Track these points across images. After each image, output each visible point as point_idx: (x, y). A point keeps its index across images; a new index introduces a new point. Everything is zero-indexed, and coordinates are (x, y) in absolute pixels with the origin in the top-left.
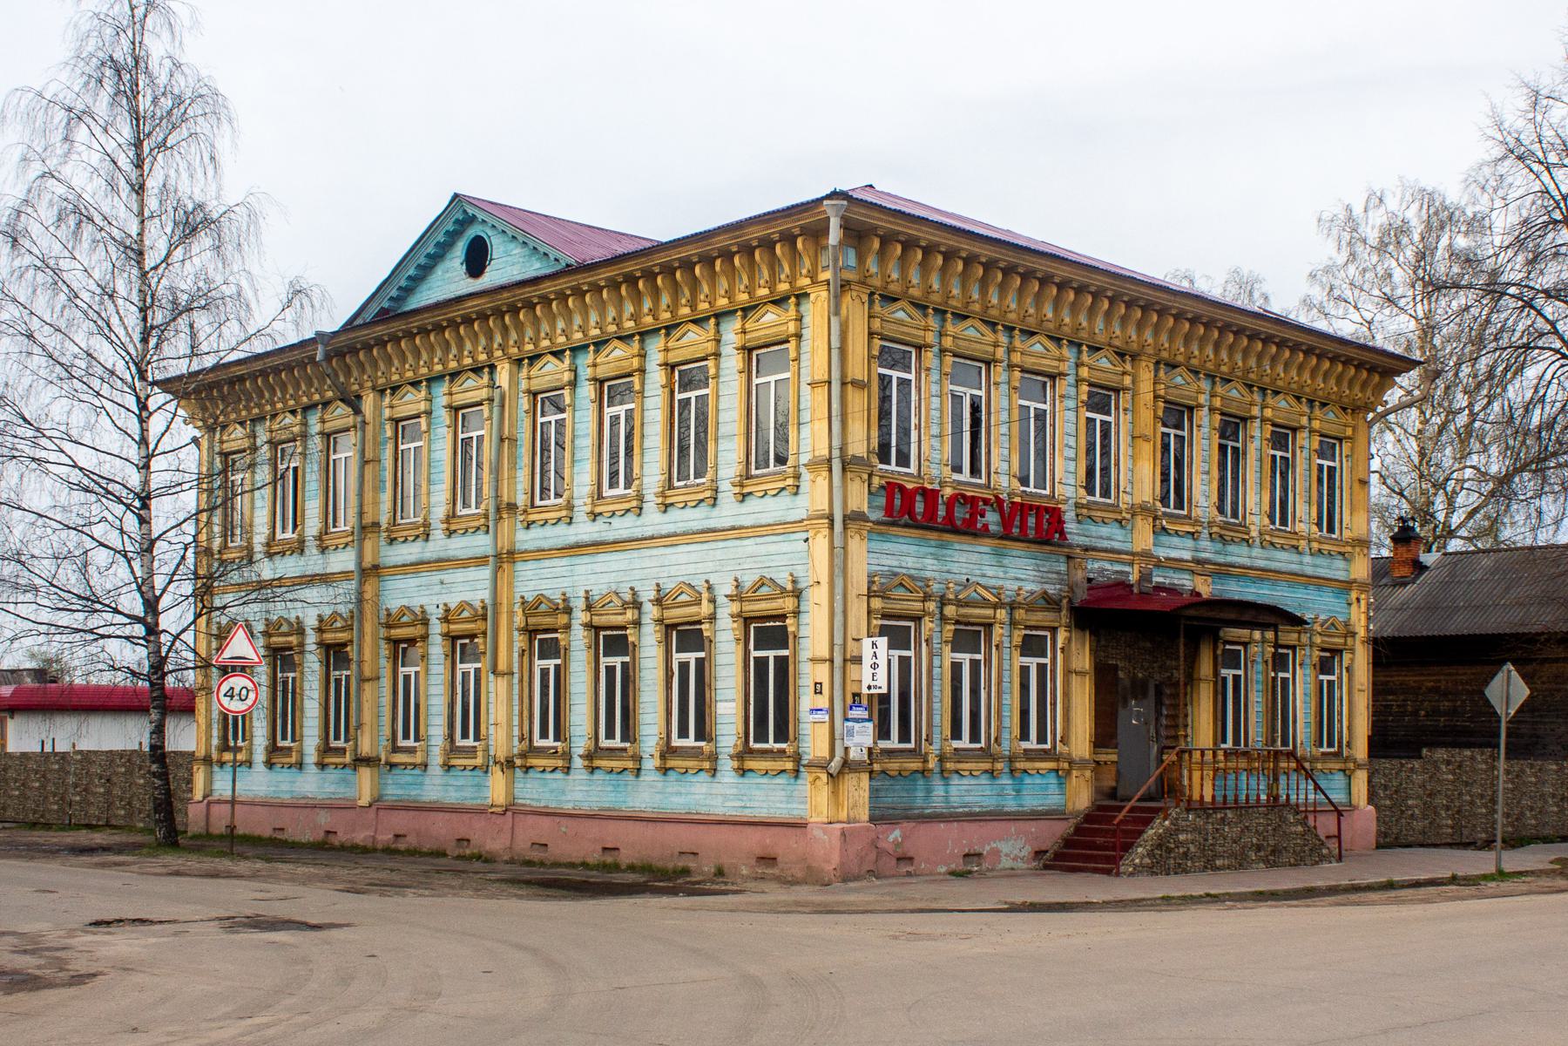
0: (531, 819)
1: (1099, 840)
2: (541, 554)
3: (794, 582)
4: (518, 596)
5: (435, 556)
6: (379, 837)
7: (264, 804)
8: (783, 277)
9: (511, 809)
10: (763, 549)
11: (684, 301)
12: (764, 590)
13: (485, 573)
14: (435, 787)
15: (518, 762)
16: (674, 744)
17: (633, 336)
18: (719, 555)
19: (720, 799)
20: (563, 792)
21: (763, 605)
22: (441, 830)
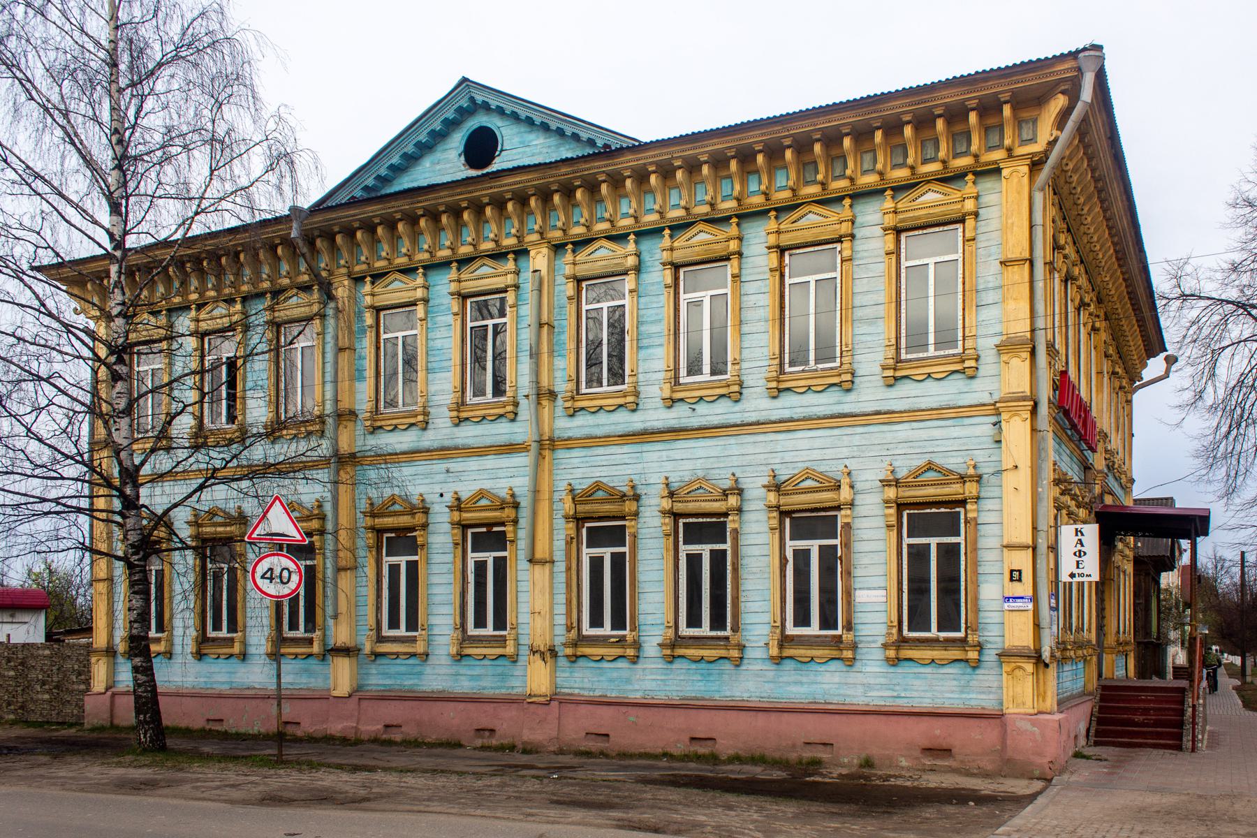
0: (584, 709)
1: (1139, 718)
2: (591, 441)
3: (633, 487)
4: (562, 485)
5: (436, 445)
6: (363, 728)
7: (193, 695)
8: (264, 276)
9: (557, 699)
10: (924, 434)
11: (193, 288)
12: (600, 494)
13: (522, 461)
14: (439, 675)
15: (563, 651)
16: (584, 633)
17: (730, 218)
18: (857, 440)
19: (860, 690)
20: (628, 681)
21: (931, 491)
22: (452, 720)
